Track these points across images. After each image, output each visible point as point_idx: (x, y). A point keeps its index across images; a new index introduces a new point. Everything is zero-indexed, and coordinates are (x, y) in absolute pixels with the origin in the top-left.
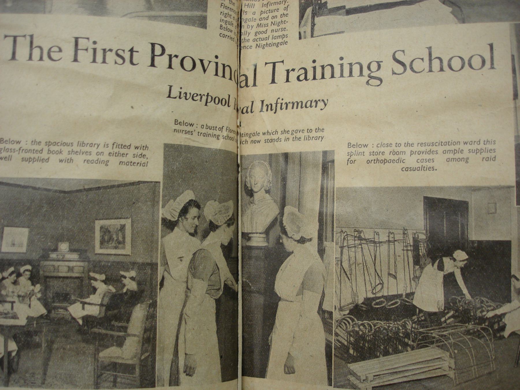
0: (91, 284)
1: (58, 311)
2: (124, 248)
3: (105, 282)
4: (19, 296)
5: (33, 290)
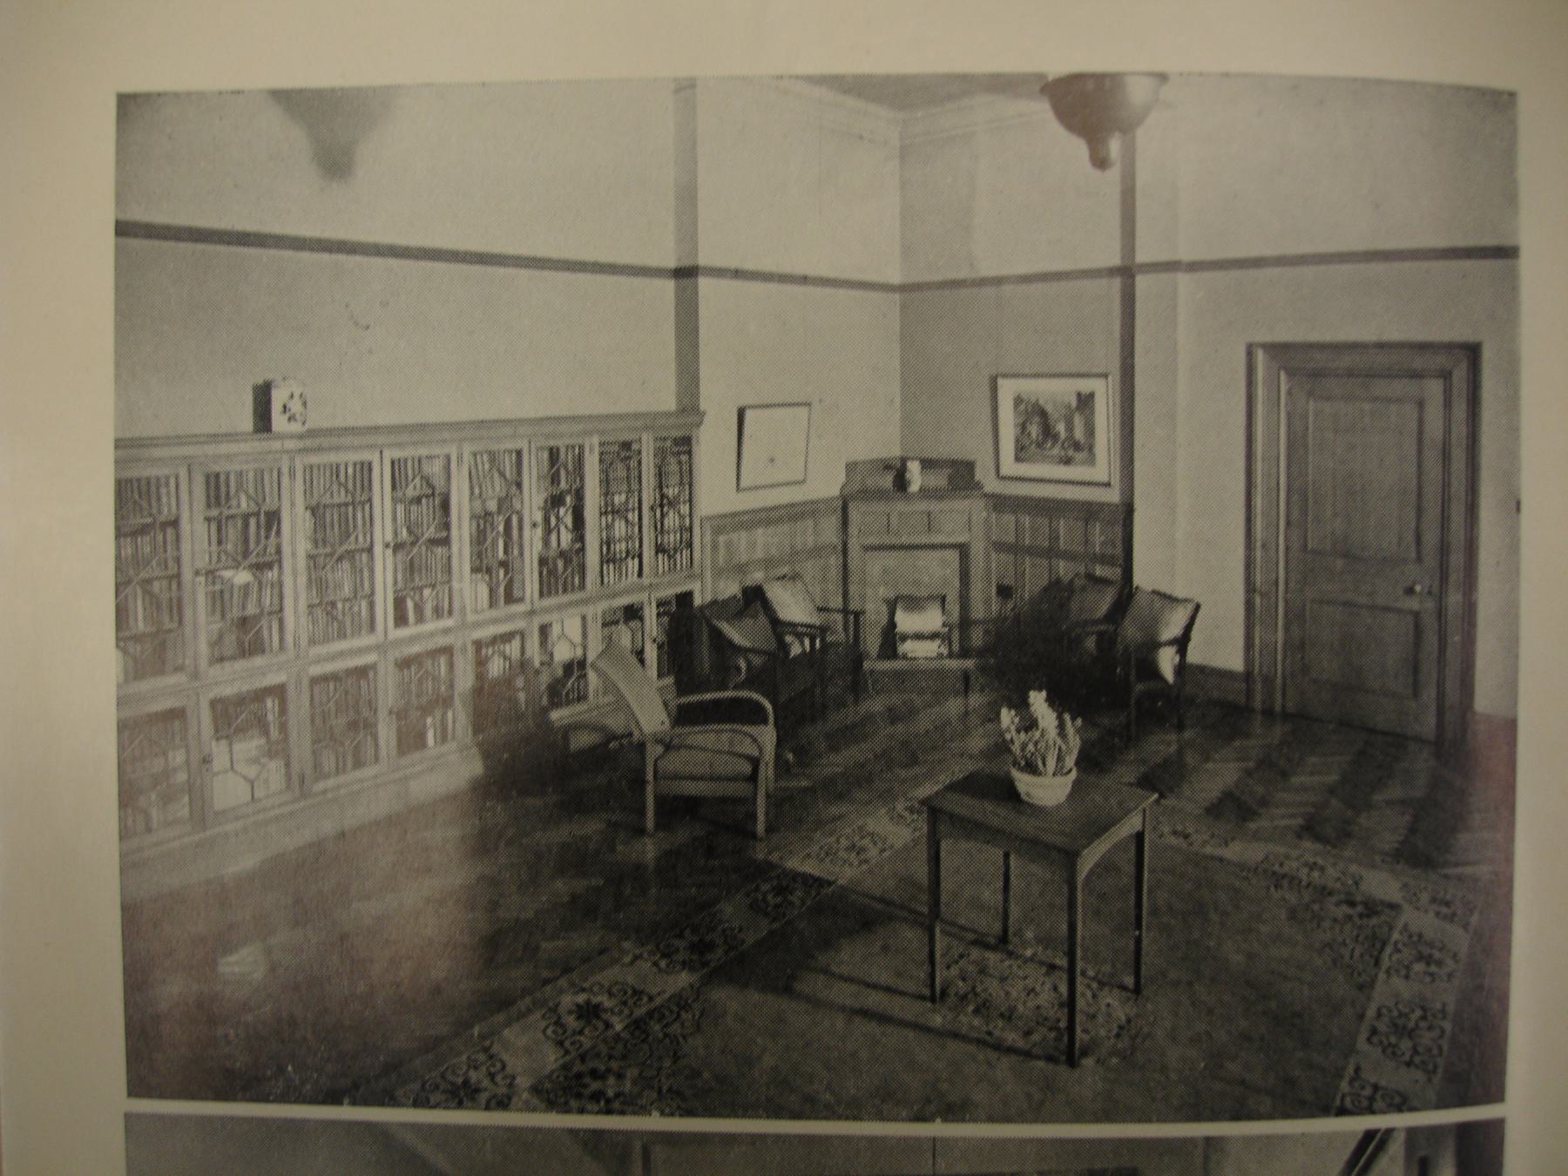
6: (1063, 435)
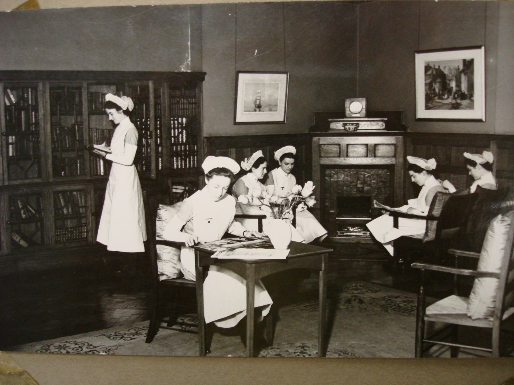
0: (410, 177)
1: (348, 231)
2: (471, 106)
3: (436, 173)
4: (273, 205)
5: (299, 194)
6: (454, 89)
